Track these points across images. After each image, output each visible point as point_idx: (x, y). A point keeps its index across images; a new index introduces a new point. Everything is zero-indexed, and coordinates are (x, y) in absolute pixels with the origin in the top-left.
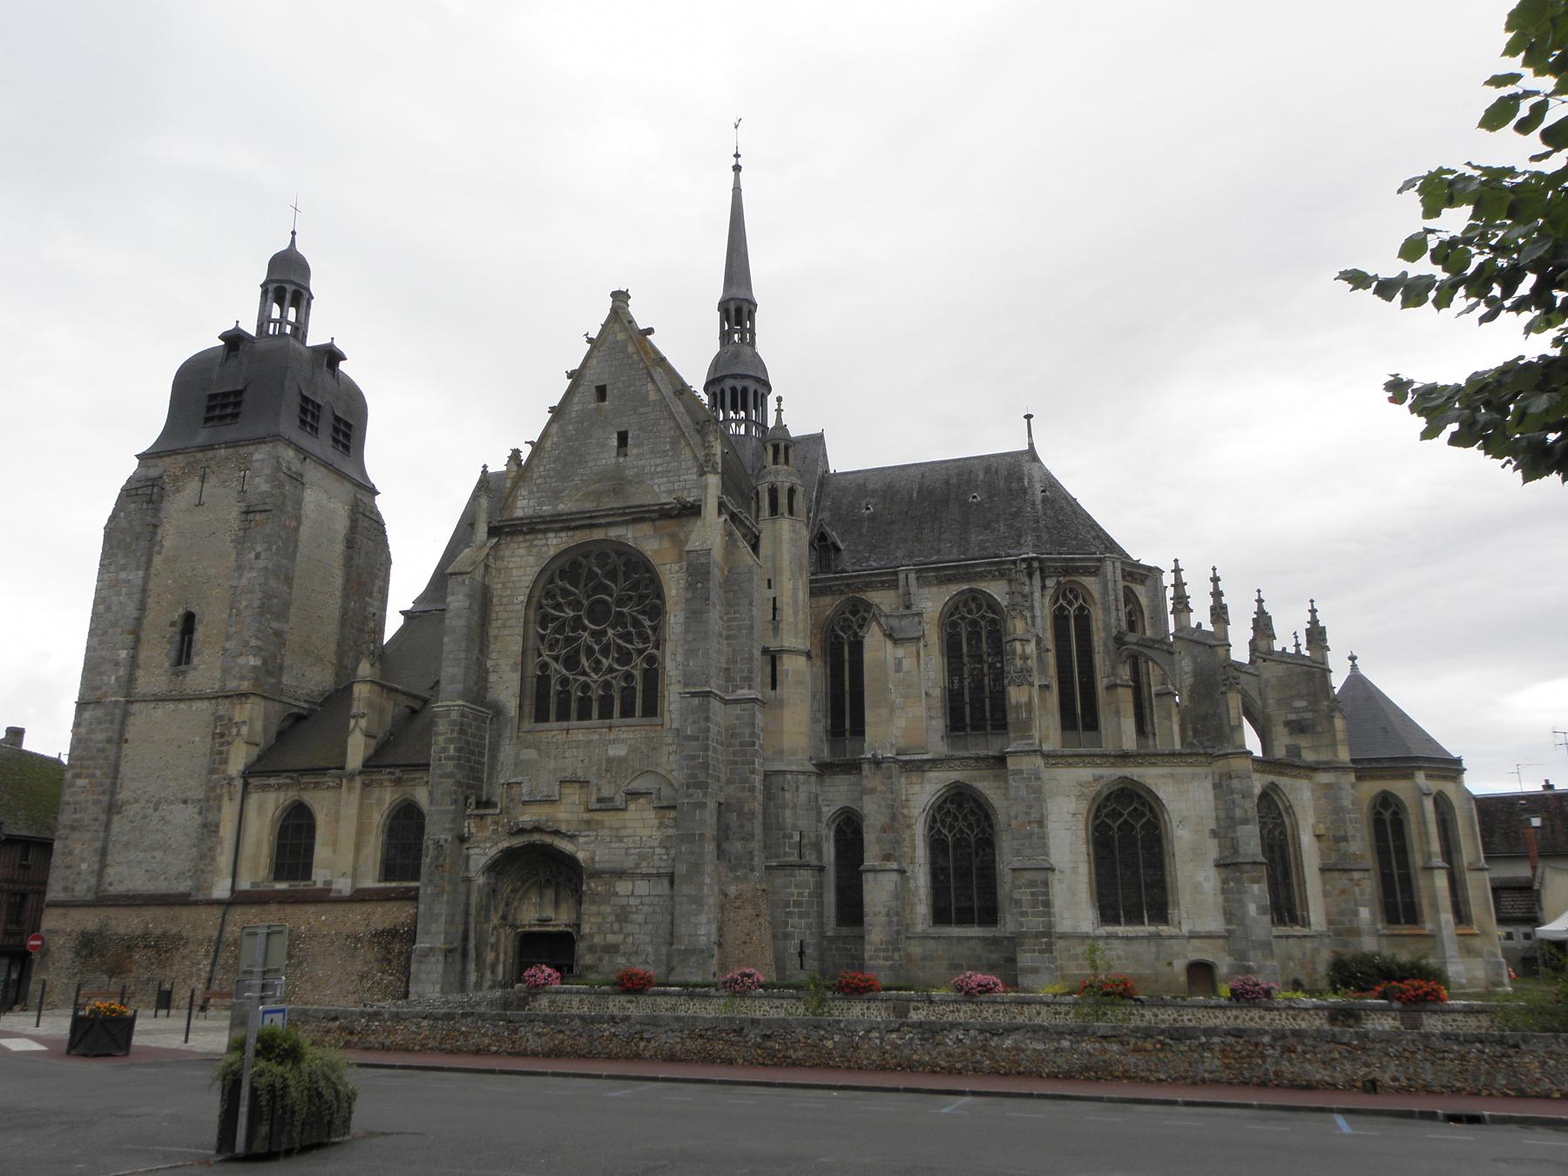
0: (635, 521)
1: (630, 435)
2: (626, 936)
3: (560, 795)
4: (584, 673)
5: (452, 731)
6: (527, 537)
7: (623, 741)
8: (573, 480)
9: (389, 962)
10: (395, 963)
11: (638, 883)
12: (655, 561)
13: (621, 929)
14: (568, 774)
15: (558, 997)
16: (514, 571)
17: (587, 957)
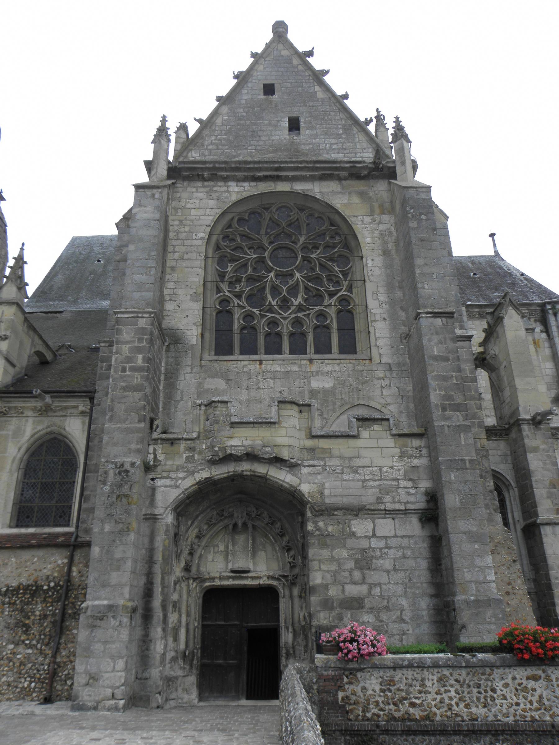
0: (323, 178)
1: (302, 120)
2: (371, 586)
3: (279, 416)
4: (271, 310)
5: (140, 340)
6: (206, 183)
7: (328, 373)
8: (246, 149)
9: (27, 629)
10: (35, 630)
11: (380, 522)
12: (346, 213)
13: (364, 578)
14: (286, 395)
15: (398, 675)
16: (193, 212)
17: (322, 615)
